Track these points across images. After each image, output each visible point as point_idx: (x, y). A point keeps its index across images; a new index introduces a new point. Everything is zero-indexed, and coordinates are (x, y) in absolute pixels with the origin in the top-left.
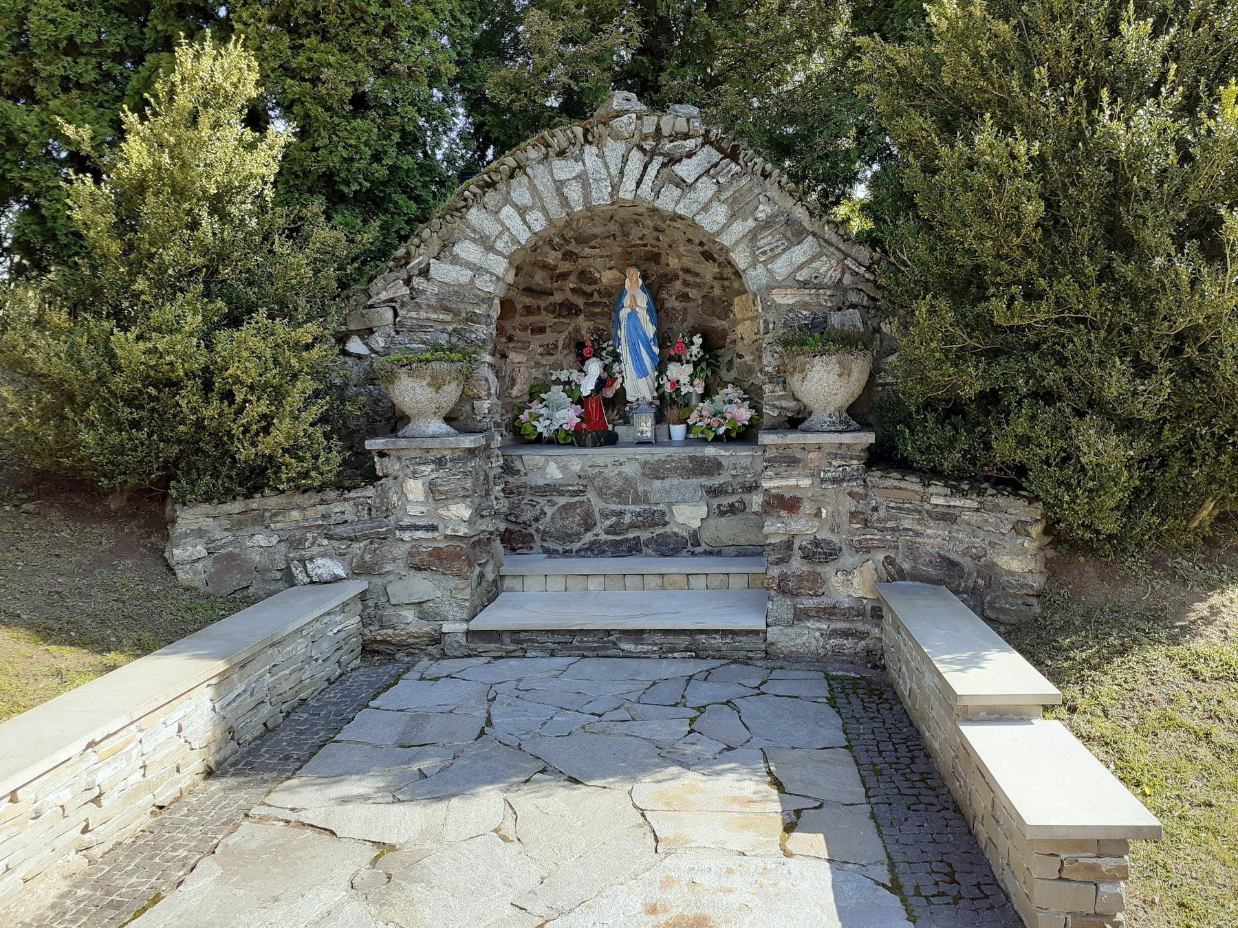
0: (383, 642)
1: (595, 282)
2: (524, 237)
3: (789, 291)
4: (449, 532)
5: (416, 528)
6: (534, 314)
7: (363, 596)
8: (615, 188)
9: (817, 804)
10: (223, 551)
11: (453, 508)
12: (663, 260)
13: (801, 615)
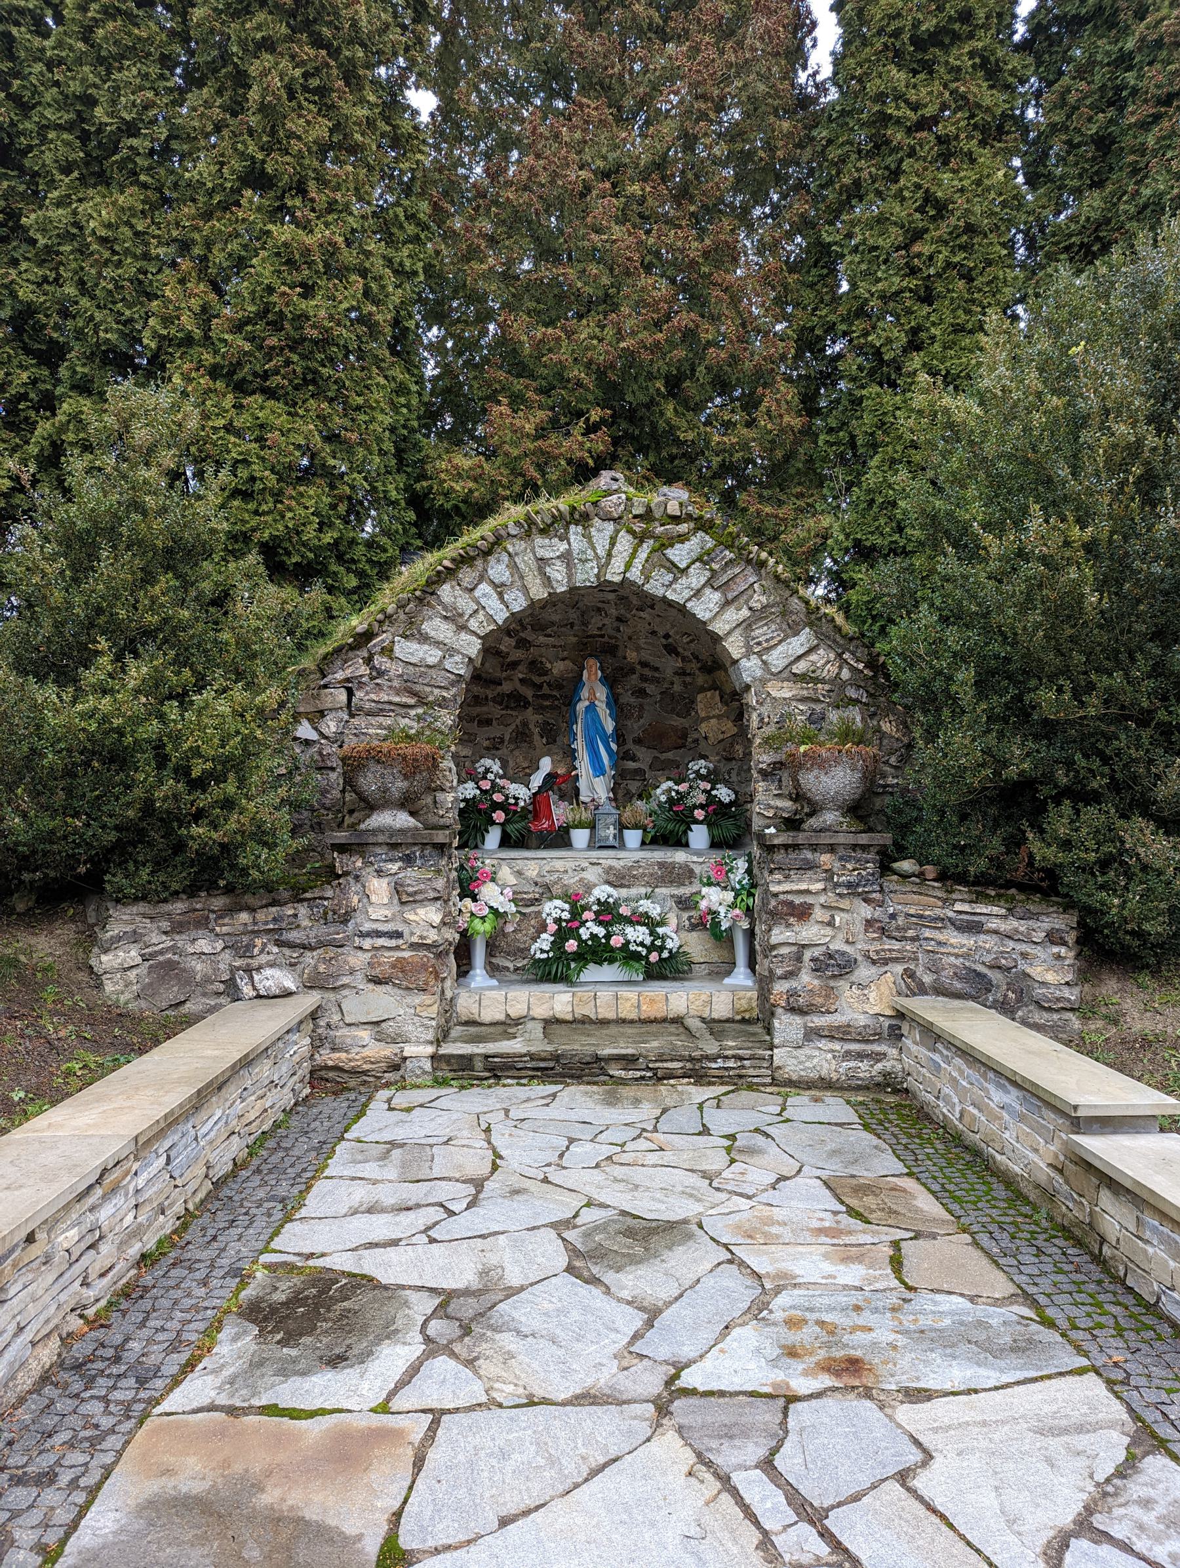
0: (336, 1068)
1: (546, 673)
2: (501, 616)
3: (785, 684)
4: (415, 939)
5: (379, 934)
6: (481, 705)
7: (314, 1016)
8: (603, 567)
9: (912, 1234)
10: (161, 958)
11: (421, 911)
12: (620, 654)
13: (812, 1034)
